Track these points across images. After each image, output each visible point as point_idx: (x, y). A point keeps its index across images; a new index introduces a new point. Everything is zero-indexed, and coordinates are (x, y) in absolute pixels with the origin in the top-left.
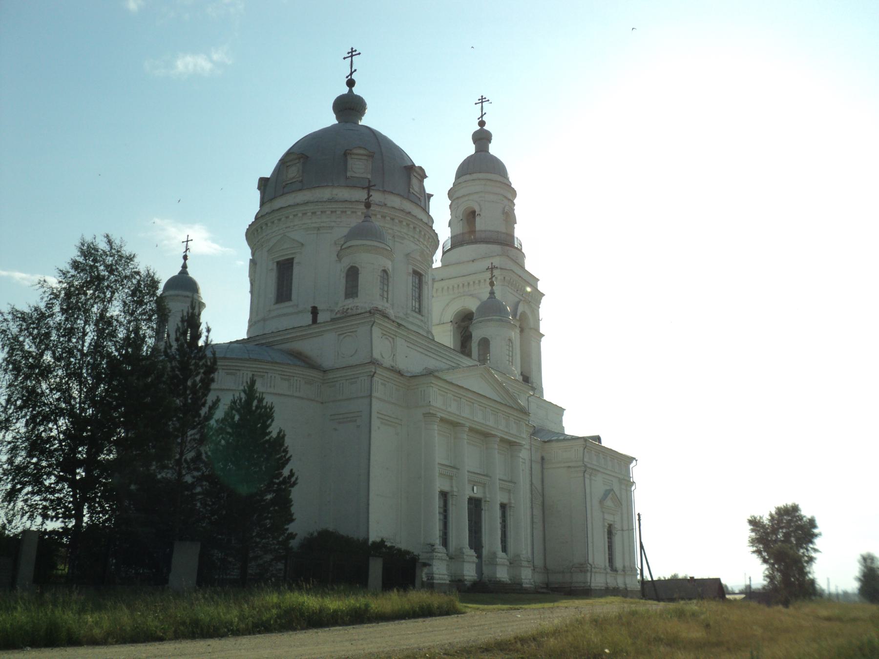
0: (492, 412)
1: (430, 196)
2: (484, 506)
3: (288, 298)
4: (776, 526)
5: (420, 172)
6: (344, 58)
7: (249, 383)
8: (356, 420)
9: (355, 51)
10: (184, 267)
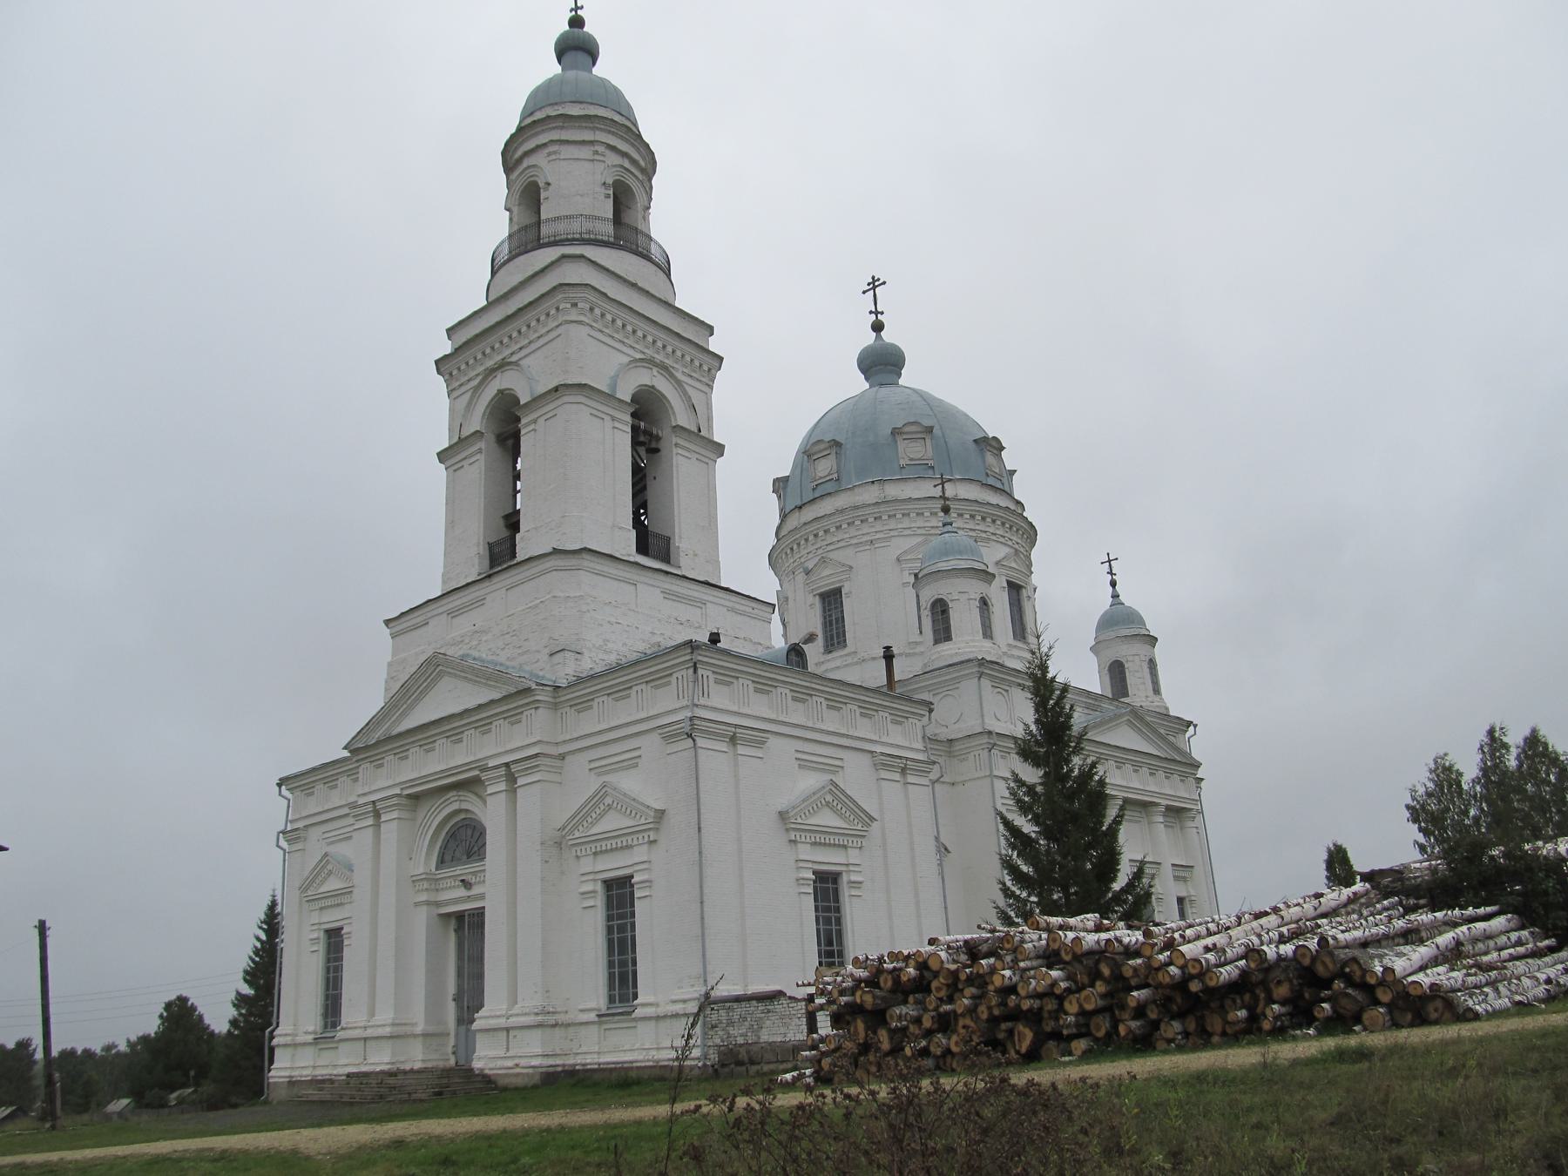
3: (948, 638)
4: (1030, 817)
5: (994, 443)
6: (864, 292)
7: (1029, 828)
8: (637, 763)
9: (878, 280)
10: (1115, 596)
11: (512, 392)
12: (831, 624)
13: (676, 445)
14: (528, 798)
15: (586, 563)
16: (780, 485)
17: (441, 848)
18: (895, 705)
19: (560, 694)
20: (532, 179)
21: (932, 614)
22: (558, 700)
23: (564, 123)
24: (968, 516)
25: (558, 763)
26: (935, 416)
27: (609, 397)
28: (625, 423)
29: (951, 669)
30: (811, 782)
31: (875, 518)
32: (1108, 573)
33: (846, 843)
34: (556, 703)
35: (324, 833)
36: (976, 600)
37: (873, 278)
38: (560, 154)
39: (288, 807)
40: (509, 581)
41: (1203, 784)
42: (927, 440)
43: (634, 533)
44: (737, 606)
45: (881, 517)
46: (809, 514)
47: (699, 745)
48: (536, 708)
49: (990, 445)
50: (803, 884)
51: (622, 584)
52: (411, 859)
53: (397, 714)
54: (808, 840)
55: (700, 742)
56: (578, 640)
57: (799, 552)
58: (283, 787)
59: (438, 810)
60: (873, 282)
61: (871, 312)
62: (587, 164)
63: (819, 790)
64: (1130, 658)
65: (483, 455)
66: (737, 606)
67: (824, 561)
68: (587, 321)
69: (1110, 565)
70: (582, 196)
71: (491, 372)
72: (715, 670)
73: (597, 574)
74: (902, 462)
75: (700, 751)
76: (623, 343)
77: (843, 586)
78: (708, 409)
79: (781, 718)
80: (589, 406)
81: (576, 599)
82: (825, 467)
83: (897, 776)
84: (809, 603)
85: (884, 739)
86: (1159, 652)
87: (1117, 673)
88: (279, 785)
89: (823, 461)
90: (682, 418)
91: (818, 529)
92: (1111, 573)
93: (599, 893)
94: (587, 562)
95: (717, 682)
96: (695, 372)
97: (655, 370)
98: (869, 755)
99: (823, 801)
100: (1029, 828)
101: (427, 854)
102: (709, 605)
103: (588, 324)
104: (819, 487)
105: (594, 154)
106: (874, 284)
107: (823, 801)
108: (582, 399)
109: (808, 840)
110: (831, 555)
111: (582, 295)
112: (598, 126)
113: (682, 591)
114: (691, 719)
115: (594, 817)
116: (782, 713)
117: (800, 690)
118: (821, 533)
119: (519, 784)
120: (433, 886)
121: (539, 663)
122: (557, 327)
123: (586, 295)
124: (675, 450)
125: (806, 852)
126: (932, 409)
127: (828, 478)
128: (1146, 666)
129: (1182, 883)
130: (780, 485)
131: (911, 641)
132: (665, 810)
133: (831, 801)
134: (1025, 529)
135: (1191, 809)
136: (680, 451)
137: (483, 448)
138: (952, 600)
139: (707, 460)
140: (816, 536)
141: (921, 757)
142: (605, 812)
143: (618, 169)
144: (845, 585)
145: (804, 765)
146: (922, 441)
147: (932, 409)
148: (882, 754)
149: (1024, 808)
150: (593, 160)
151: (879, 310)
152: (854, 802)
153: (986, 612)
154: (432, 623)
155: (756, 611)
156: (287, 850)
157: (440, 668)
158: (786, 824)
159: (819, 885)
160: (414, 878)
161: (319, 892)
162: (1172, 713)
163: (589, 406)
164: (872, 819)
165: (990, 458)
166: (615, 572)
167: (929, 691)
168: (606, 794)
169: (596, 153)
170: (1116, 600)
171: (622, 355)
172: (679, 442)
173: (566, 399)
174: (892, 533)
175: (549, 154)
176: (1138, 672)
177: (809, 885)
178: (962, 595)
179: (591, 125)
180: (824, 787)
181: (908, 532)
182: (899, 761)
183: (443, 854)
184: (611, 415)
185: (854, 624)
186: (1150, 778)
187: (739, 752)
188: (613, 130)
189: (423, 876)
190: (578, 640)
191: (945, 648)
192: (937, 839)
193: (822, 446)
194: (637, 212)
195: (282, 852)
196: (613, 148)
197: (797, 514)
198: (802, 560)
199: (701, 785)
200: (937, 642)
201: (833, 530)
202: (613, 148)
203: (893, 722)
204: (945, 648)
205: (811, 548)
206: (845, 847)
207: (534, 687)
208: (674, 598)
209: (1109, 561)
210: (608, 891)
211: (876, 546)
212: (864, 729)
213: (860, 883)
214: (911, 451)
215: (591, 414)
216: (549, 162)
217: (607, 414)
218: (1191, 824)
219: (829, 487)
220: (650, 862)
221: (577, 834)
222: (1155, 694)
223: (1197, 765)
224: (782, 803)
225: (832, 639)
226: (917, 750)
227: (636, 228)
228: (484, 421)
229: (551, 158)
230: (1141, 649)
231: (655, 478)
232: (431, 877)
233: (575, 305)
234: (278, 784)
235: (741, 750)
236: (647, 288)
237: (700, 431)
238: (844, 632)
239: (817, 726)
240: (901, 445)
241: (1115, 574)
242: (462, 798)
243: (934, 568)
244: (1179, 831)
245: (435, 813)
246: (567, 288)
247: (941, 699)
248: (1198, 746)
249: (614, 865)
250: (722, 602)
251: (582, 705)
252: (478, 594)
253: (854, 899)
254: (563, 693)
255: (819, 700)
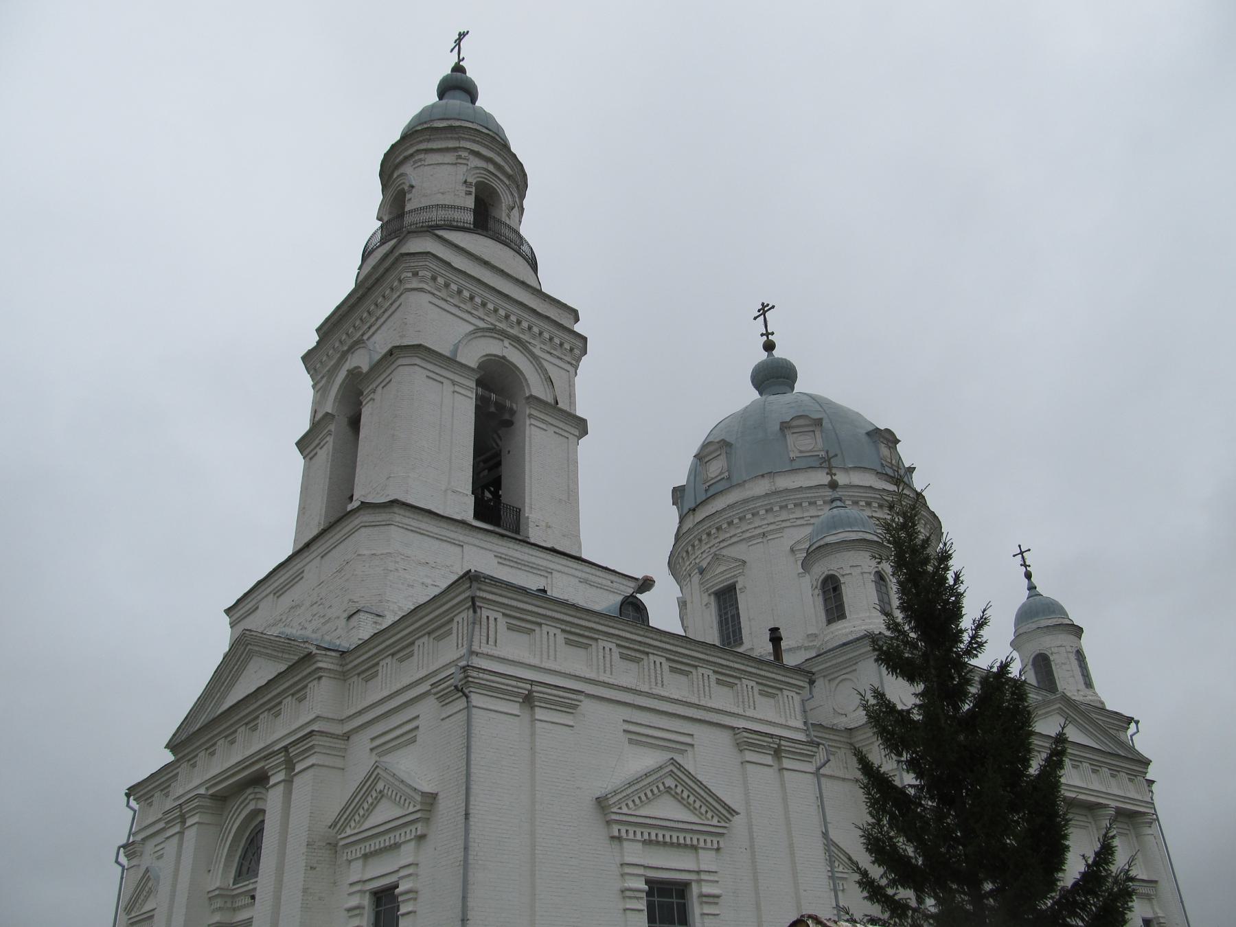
0: (1111, 772)
1: (911, 470)
2: (844, 619)
5: (887, 436)
6: (755, 318)
7: (907, 780)
10: (1032, 588)
11: (360, 370)
12: (727, 623)
13: (530, 416)
14: (303, 784)
15: (398, 518)
16: (678, 494)
17: (240, 857)
18: (762, 673)
19: (348, 661)
20: (401, 187)
21: (824, 592)
22: (346, 668)
23: (430, 135)
24: (863, 503)
25: (340, 744)
26: (825, 411)
27: (449, 362)
28: (468, 388)
29: (847, 648)
30: (645, 760)
31: (767, 511)
32: (1021, 565)
33: (695, 842)
34: (344, 673)
35: (155, 846)
36: (870, 573)
37: (763, 304)
38: (424, 160)
39: (133, 819)
40: (320, 550)
41: (1154, 787)
42: (817, 433)
43: (473, 498)
44: (590, 577)
45: (772, 509)
46: (700, 515)
47: (474, 703)
48: (320, 678)
49: (883, 437)
50: (630, 898)
51: (444, 545)
52: (209, 871)
53: (212, 705)
54: (639, 837)
55: (476, 700)
56: (380, 601)
57: (694, 553)
58: (132, 798)
59: (237, 813)
60: (763, 309)
61: (762, 335)
62: (449, 168)
63: (654, 771)
64: (1055, 650)
65: (332, 437)
66: (590, 577)
67: (717, 558)
68: (429, 289)
69: (1023, 557)
70: (443, 194)
71: (344, 356)
72: (508, 612)
73: (412, 531)
74: (792, 455)
75: (474, 711)
76: (471, 314)
77: (737, 582)
78: (570, 386)
79: (602, 678)
80: (425, 368)
81: (381, 557)
82: (715, 468)
83: (768, 760)
84: (704, 603)
85: (749, 713)
86: (1086, 643)
87: (1042, 663)
88: (128, 795)
89: (714, 463)
90: (536, 387)
91: (710, 527)
92: (1025, 565)
93: (367, 908)
94: (399, 516)
95: (510, 628)
96: (555, 349)
97: (506, 343)
98: (730, 732)
99: (662, 788)
100: (907, 780)
101: (225, 865)
102: (555, 574)
103: (429, 292)
104: (711, 488)
105: (457, 159)
106: (764, 310)
107: (662, 788)
108: (418, 361)
109: (639, 837)
110: (724, 552)
111: (424, 263)
112: (463, 136)
113: (522, 557)
114: (464, 669)
115: (365, 808)
116: (605, 672)
117: (631, 646)
118: (713, 531)
119: (296, 771)
120: (229, 905)
121: (337, 631)
122: (399, 297)
123: (427, 263)
124: (528, 422)
125: (634, 853)
126: (821, 406)
127: (719, 478)
128: (1073, 657)
129: (1146, 901)
130: (678, 494)
131: (810, 632)
132: (437, 794)
133: (673, 787)
134: (928, 519)
135: (1144, 814)
136: (533, 421)
137: (333, 430)
138: (843, 575)
139: (566, 434)
140: (709, 534)
141: (801, 737)
142: (378, 800)
143: (482, 172)
144: (739, 579)
145: (636, 739)
146: (811, 434)
147: (821, 406)
148: (746, 730)
149: (894, 744)
150: (456, 164)
151: (769, 331)
152: (705, 788)
153: (883, 588)
154: (261, 605)
155: (615, 585)
156: (126, 867)
157: (249, 647)
158: (605, 815)
159: (656, 899)
160: (210, 895)
161: (141, 912)
162: (1108, 708)
163: (425, 368)
164: (733, 812)
165: (885, 451)
166: (436, 530)
167: (824, 676)
168: (378, 778)
169: (459, 157)
170: (1033, 592)
171: (465, 323)
172: (532, 413)
173: (400, 361)
174: (784, 524)
175: (415, 162)
176: (1064, 664)
177: (641, 898)
178: (855, 568)
179: (456, 136)
180: (661, 768)
181: (799, 522)
182: (771, 740)
183: (242, 864)
184: (451, 380)
185: (750, 620)
186: (1093, 776)
187: (537, 717)
188: (477, 139)
189: (217, 892)
190: (380, 601)
191: (839, 627)
192: (825, 835)
193: (711, 448)
194: (502, 210)
195: (120, 868)
196: (477, 154)
197: (692, 517)
198: (697, 561)
199: (473, 756)
200: (830, 621)
201: (725, 526)
202: (477, 154)
203: (761, 693)
204: (839, 627)
205: (705, 547)
206: (695, 848)
207: (315, 651)
208: (512, 564)
209: (1022, 553)
210: (377, 907)
211: (769, 537)
212: (721, 698)
213: (718, 897)
214: (801, 444)
215: (427, 377)
216: (414, 168)
217: (448, 379)
218: (1149, 831)
219: (720, 487)
220: (417, 864)
221: (349, 831)
222: (1087, 688)
223: (1146, 763)
224: (602, 786)
225: (729, 638)
226: (796, 729)
227: (501, 221)
228: (337, 404)
229: (416, 165)
230: (1066, 640)
231: (509, 452)
232: (225, 893)
233: (416, 274)
234: (126, 794)
235: (540, 714)
236: (502, 267)
237: (557, 403)
238: (740, 629)
239: (654, 691)
240: (791, 439)
241: (1029, 566)
242: (258, 796)
243: (822, 543)
244: (1135, 838)
245: (235, 816)
246: (408, 258)
247: (837, 685)
248: (1143, 743)
249: (380, 871)
250: (573, 572)
251: (369, 672)
252: (296, 568)
253: (707, 920)
254: (350, 659)
255: (659, 660)
